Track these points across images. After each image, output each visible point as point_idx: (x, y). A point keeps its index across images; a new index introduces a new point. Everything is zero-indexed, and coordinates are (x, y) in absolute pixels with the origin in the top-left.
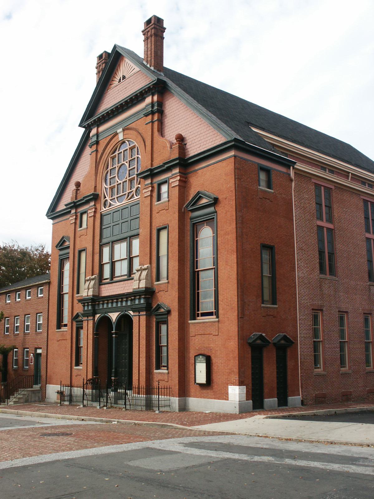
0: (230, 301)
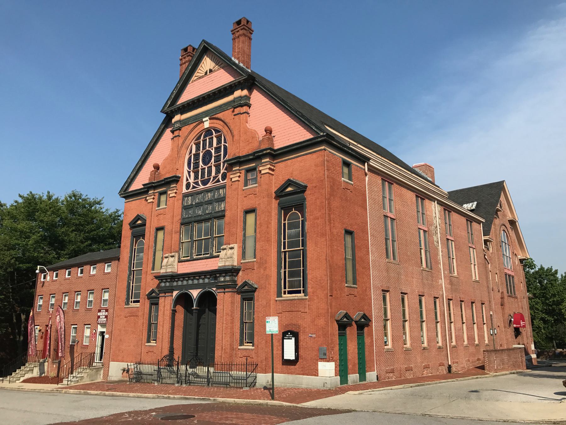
0: (320, 280)
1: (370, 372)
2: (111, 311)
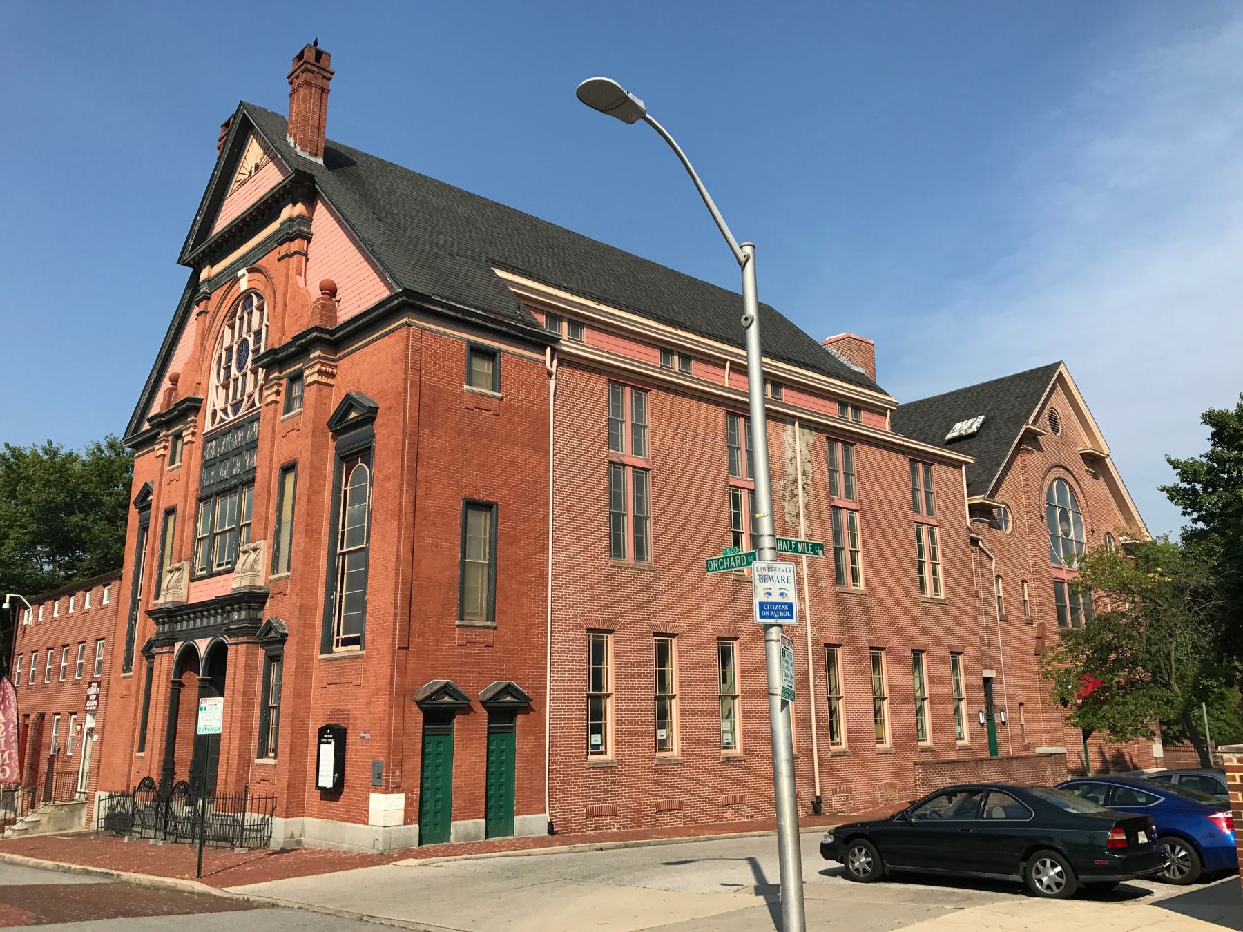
0: (384, 614)
1: (527, 814)
2: (104, 684)
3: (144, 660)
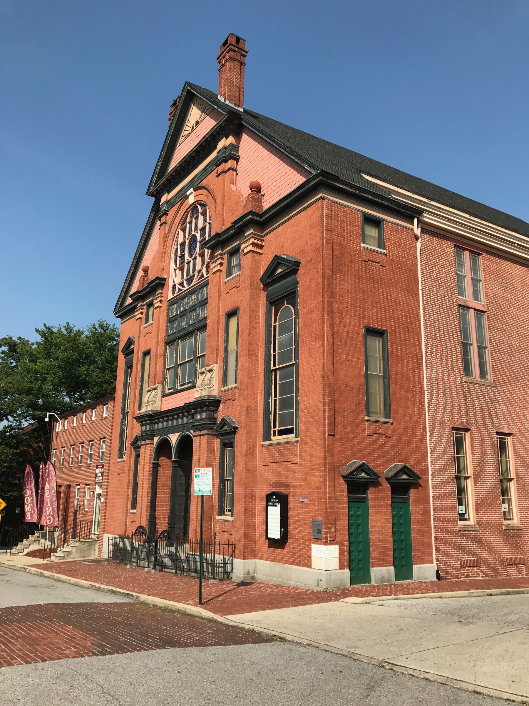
0: (314, 410)
1: (421, 564)
2: (106, 466)
3: (133, 450)
